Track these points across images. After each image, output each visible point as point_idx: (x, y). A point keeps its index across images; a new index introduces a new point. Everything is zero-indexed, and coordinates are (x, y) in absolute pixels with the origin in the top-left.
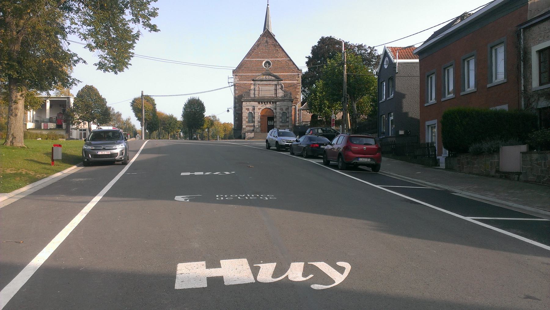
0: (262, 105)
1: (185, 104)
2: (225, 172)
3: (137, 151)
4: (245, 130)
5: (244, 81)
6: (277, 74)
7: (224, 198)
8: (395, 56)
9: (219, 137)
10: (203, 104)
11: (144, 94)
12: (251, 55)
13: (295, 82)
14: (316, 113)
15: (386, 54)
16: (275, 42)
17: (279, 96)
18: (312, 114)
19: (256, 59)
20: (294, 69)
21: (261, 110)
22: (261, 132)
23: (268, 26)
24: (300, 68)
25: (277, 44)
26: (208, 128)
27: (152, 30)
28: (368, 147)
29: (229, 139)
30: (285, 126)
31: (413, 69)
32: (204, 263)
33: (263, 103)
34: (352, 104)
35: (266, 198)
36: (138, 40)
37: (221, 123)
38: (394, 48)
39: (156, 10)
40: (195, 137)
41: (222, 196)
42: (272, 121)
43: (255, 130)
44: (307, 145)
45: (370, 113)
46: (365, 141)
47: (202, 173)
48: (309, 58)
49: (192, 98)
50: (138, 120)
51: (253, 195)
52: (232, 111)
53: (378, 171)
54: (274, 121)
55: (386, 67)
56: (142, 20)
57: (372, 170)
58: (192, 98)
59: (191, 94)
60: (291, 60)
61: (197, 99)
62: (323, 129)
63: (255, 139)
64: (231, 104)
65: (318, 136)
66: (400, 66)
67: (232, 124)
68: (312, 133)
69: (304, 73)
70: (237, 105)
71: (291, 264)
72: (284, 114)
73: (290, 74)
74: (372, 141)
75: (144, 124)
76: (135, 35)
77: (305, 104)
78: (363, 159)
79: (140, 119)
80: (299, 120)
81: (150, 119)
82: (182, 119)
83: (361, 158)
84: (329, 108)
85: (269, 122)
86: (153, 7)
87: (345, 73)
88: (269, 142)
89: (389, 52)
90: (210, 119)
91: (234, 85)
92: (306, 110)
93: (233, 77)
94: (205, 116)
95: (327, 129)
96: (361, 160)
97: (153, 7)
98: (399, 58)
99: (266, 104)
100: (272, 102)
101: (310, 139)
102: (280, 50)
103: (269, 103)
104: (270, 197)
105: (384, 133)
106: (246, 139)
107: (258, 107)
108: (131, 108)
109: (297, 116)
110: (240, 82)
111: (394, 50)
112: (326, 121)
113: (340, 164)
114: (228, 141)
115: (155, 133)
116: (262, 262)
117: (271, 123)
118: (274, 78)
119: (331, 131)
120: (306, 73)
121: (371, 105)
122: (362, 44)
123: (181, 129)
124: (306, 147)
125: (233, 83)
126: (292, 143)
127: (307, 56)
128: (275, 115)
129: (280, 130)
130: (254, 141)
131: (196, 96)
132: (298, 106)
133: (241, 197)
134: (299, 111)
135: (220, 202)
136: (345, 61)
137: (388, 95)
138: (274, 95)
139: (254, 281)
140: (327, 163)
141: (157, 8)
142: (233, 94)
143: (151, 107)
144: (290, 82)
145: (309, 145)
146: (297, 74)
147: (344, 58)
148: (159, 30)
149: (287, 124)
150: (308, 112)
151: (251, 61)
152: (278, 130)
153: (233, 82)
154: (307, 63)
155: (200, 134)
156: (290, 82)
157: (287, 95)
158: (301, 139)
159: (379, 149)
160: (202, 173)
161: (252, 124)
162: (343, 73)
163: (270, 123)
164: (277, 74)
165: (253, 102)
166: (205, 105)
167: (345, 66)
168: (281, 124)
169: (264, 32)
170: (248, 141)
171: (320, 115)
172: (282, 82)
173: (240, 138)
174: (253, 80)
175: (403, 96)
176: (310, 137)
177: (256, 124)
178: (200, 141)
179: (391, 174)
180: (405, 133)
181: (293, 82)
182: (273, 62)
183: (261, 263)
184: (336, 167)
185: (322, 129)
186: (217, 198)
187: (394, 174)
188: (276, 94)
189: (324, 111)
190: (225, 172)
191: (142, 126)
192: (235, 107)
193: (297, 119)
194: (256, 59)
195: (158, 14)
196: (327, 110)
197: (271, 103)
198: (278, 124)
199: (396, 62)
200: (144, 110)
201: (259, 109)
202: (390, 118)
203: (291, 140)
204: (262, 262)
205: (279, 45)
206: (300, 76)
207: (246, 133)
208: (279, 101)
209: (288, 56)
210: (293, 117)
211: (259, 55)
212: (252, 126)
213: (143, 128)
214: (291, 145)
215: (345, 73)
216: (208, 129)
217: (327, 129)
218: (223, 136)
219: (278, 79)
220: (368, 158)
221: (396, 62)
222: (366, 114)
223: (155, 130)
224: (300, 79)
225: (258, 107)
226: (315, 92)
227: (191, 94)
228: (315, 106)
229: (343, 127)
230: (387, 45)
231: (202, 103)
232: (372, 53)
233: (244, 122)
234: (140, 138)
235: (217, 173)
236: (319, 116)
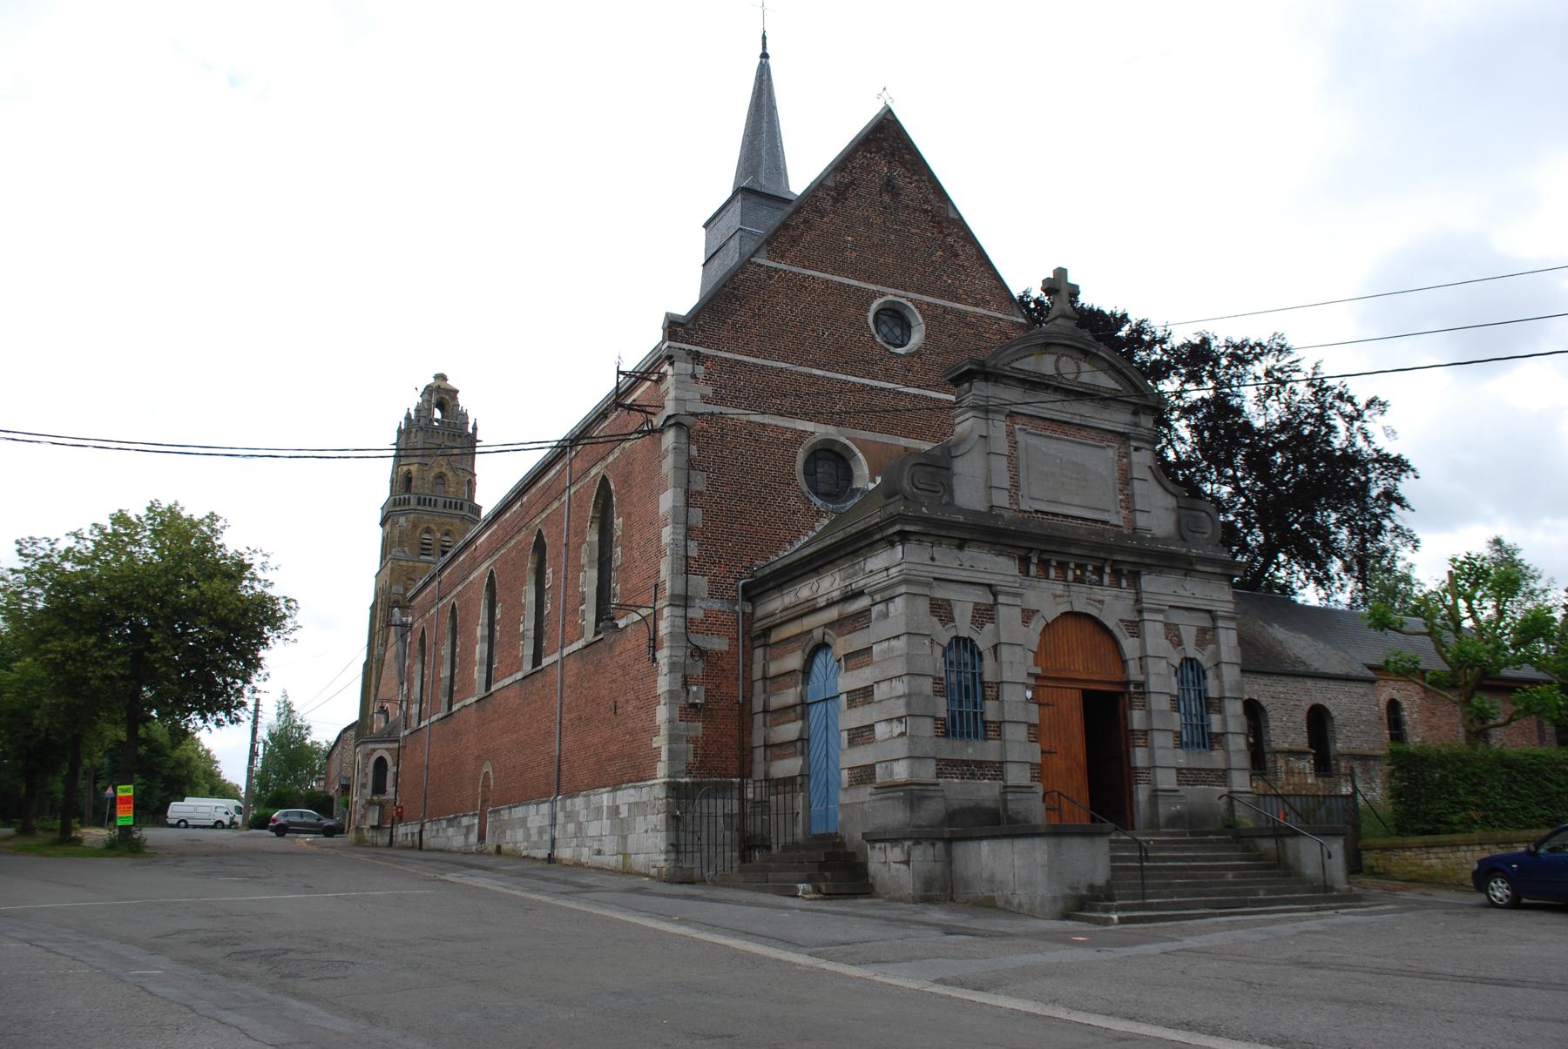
19: (828, 276)
194: (828, 276)
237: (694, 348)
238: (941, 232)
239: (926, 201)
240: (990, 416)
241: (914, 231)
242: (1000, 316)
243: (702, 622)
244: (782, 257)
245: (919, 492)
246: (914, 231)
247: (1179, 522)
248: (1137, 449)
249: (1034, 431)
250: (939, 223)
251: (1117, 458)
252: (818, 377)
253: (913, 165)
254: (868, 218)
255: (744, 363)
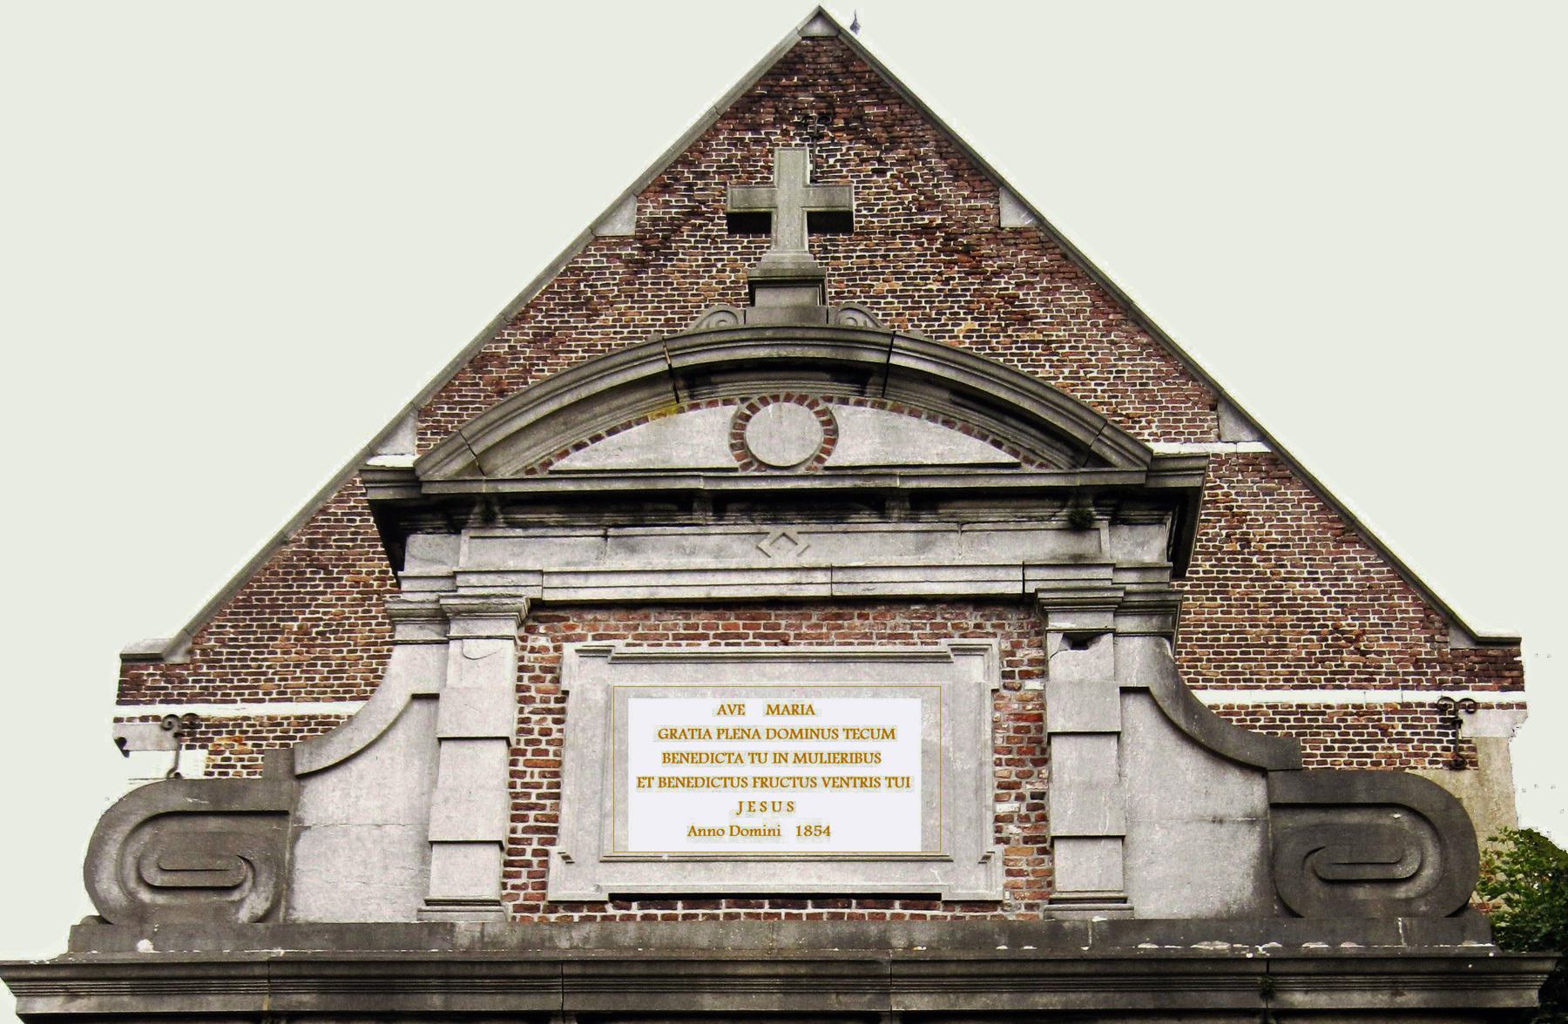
237: (181, 710)
238: (975, 271)
239: (933, 203)
240: (455, 629)
241: (879, 286)
245: (161, 899)
246: (879, 286)
247: (1270, 864)
248: (1079, 640)
249: (645, 649)
250: (967, 250)
251: (996, 682)
253: (887, 128)
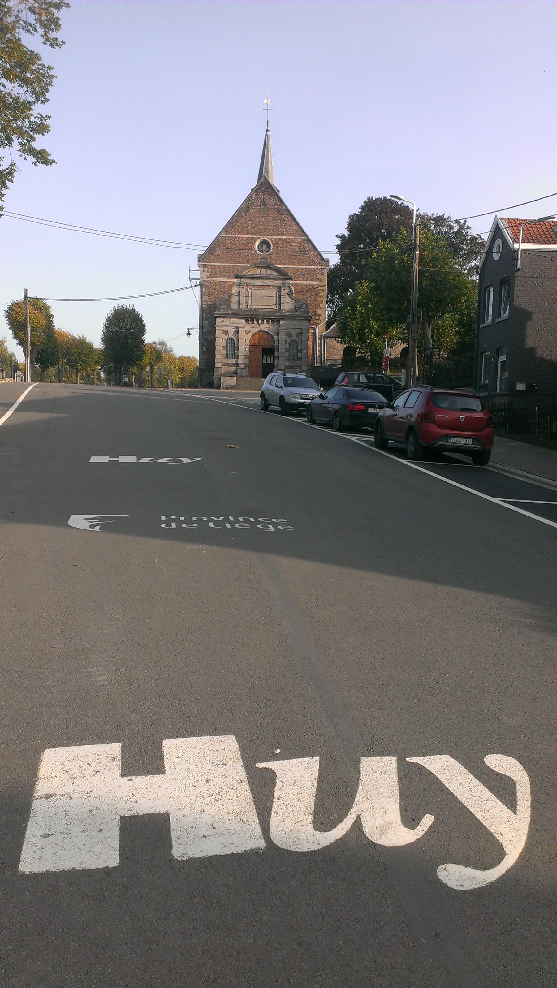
0: (253, 325)
1: (107, 317)
2: (180, 459)
3: (10, 405)
4: (220, 372)
5: (220, 277)
6: (281, 266)
7: (179, 523)
8: (515, 237)
9: (172, 383)
10: (141, 318)
11: (30, 295)
12: (233, 227)
13: (314, 283)
14: (353, 345)
15: (497, 232)
16: (279, 204)
17: (284, 310)
18: (346, 346)
19: (243, 236)
20: (314, 259)
21: (250, 334)
22: (250, 377)
23: (267, 172)
24: (325, 257)
25: (284, 208)
26: (152, 365)
27: (39, 162)
28: (468, 414)
29: (190, 388)
30: (296, 366)
31: (549, 262)
32: (115, 748)
33: (255, 322)
34: (423, 328)
35: (271, 527)
36: (13, 182)
37: (175, 357)
38: (514, 220)
39: (45, 120)
40: (127, 380)
41: (173, 517)
42: (270, 357)
43: (238, 372)
44: (341, 405)
45: (453, 347)
46: (461, 402)
47: (133, 459)
48: (342, 237)
49: (120, 305)
50: (19, 344)
51: (241, 519)
52: (196, 335)
53: (485, 463)
54: (274, 356)
55: (496, 257)
56: (19, 141)
57: (471, 462)
58: (120, 305)
59: (119, 299)
60: (309, 240)
61: (131, 308)
62: (369, 375)
63: (238, 389)
64: (194, 320)
65: (363, 390)
66: (524, 255)
67: (196, 360)
68: (347, 383)
69: (332, 267)
70: (206, 323)
71: (359, 762)
72: (293, 344)
73: (307, 267)
74: (475, 404)
75: (29, 352)
76: (4, 171)
77: (332, 327)
78: (458, 439)
79: (22, 343)
80: (320, 357)
81: (41, 343)
82: (102, 346)
83: (454, 437)
84: (378, 334)
85: (265, 357)
86: (39, 114)
87: (417, 267)
88: (266, 397)
89: (504, 227)
90: (154, 349)
91: (201, 285)
92: (335, 338)
93: (198, 268)
94: (146, 342)
95: (377, 375)
96: (453, 440)
97: (39, 114)
98: (524, 242)
99: (260, 322)
100: (271, 319)
101: (349, 395)
102: (288, 220)
103: (265, 323)
104: (280, 524)
105: (485, 387)
106: (221, 388)
107: (245, 329)
108: (6, 321)
109: (318, 348)
110: (212, 279)
111: (514, 224)
112: (372, 361)
113: (411, 449)
114: (189, 392)
115: (52, 370)
116: (278, 751)
117: (268, 360)
118: (277, 274)
119: (383, 380)
120: (336, 266)
121: (457, 332)
122: (444, 214)
123: (101, 365)
124: (340, 409)
125: (198, 281)
126: (312, 399)
127: (340, 235)
128: (277, 345)
129: (288, 375)
130: (236, 393)
131: (129, 304)
132: (320, 329)
133: (215, 523)
134: (321, 338)
135: (169, 535)
136: (418, 242)
137: (497, 312)
138: (275, 308)
139: (262, 844)
140: (382, 444)
141: (46, 116)
142: (199, 303)
143: (43, 321)
144: (305, 282)
145: (344, 407)
146: (320, 267)
147: (416, 237)
148: (53, 161)
149: (299, 363)
150: (338, 342)
151: (234, 240)
152: (285, 375)
153: (198, 279)
154: (338, 247)
155: (135, 375)
156: (305, 282)
157: (300, 307)
158: (330, 394)
159: (490, 421)
160: (133, 459)
161: (234, 361)
162: (411, 267)
163: (267, 360)
164: (281, 266)
165: (235, 318)
166: (145, 321)
167: (417, 252)
168: (287, 363)
169: (258, 183)
170: (227, 393)
171: (361, 348)
172: (291, 282)
173: (210, 385)
174: (237, 277)
175: (526, 316)
176: (347, 390)
177: (241, 361)
178: (135, 390)
179: (513, 470)
180: (527, 387)
181: (311, 283)
182: (276, 242)
183: (276, 758)
184: (402, 453)
185: (366, 376)
186: (163, 522)
187: (520, 472)
188: (280, 304)
189: (368, 341)
190: (180, 459)
191: (26, 356)
192: (201, 327)
193: (318, 354)
194: (243, 236)
195: (50, 128)
196: (375, 339)
197: (270, 323)
198: (282, 362)
199: (518, 249)
200: (29, 326)
201: (247, 332)
202: (500, 357)
203: (309, 395)
204: (278, 751)
205: (287, 210)
206: (326, 271)
207: (222, 377)
208: (284, 318)
209: (303, 231)
210: (310, 351)
211: (248, 228)
212: (233, 364)
213: (28, 361)
214: (310, 404)
215: (417, 267)
216: (151, 367)
217: (377, 375)
218: (178, 380)
219: (284, 275)
220: (467, 438)
221: (518, 249)
222: (447, 349)
223: (52, 364)
224: (325, 278)
225: (245, 329)
226: (352, 303)
227: (119, 299)
228: (352, 330)
229: (408, 373)
230: (500, 215)
231: (140, 316)
232: (463, 233)
233: (218, 357)
234: (22, 377)
235: (164, 460)
236: (358, 350)
237: (204, 263)
238: (280, 214)
242: (298, 238)
243: (207, 332)
244: (229, 233)
252: (239, 266)
254: (256, 215)
255: (218, 265)
